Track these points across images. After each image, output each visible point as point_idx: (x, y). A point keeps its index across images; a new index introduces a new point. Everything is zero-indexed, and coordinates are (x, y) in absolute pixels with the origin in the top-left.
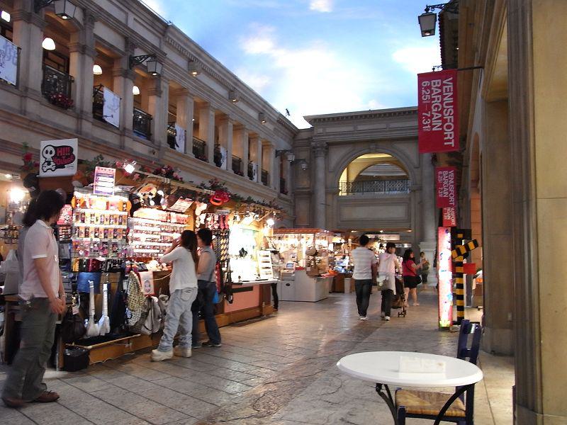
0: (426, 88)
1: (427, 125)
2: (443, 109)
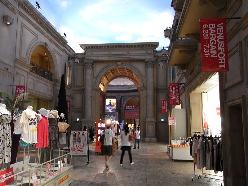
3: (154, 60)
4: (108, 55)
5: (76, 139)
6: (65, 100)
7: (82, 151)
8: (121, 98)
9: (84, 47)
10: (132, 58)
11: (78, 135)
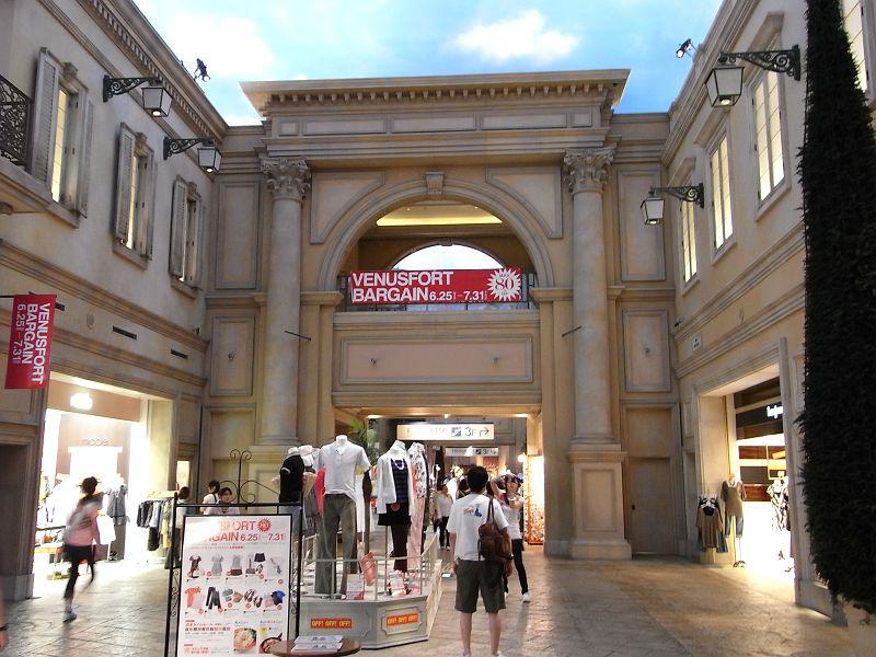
3: (607, 153)
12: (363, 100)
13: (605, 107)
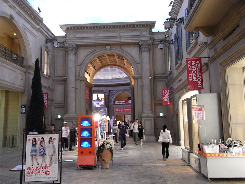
0: (190, 64)
1: (191, 79)
2: (197, 73)
3: (150, 42)
4: (94, 38)
5: (36, 151)
6: (41, 91)
7: (48, 173)
8: (109, 93)
9: (65, 28)
10: (123, 40)
11: (41, 142)
12: (116, 28)
13: (150, 31)
